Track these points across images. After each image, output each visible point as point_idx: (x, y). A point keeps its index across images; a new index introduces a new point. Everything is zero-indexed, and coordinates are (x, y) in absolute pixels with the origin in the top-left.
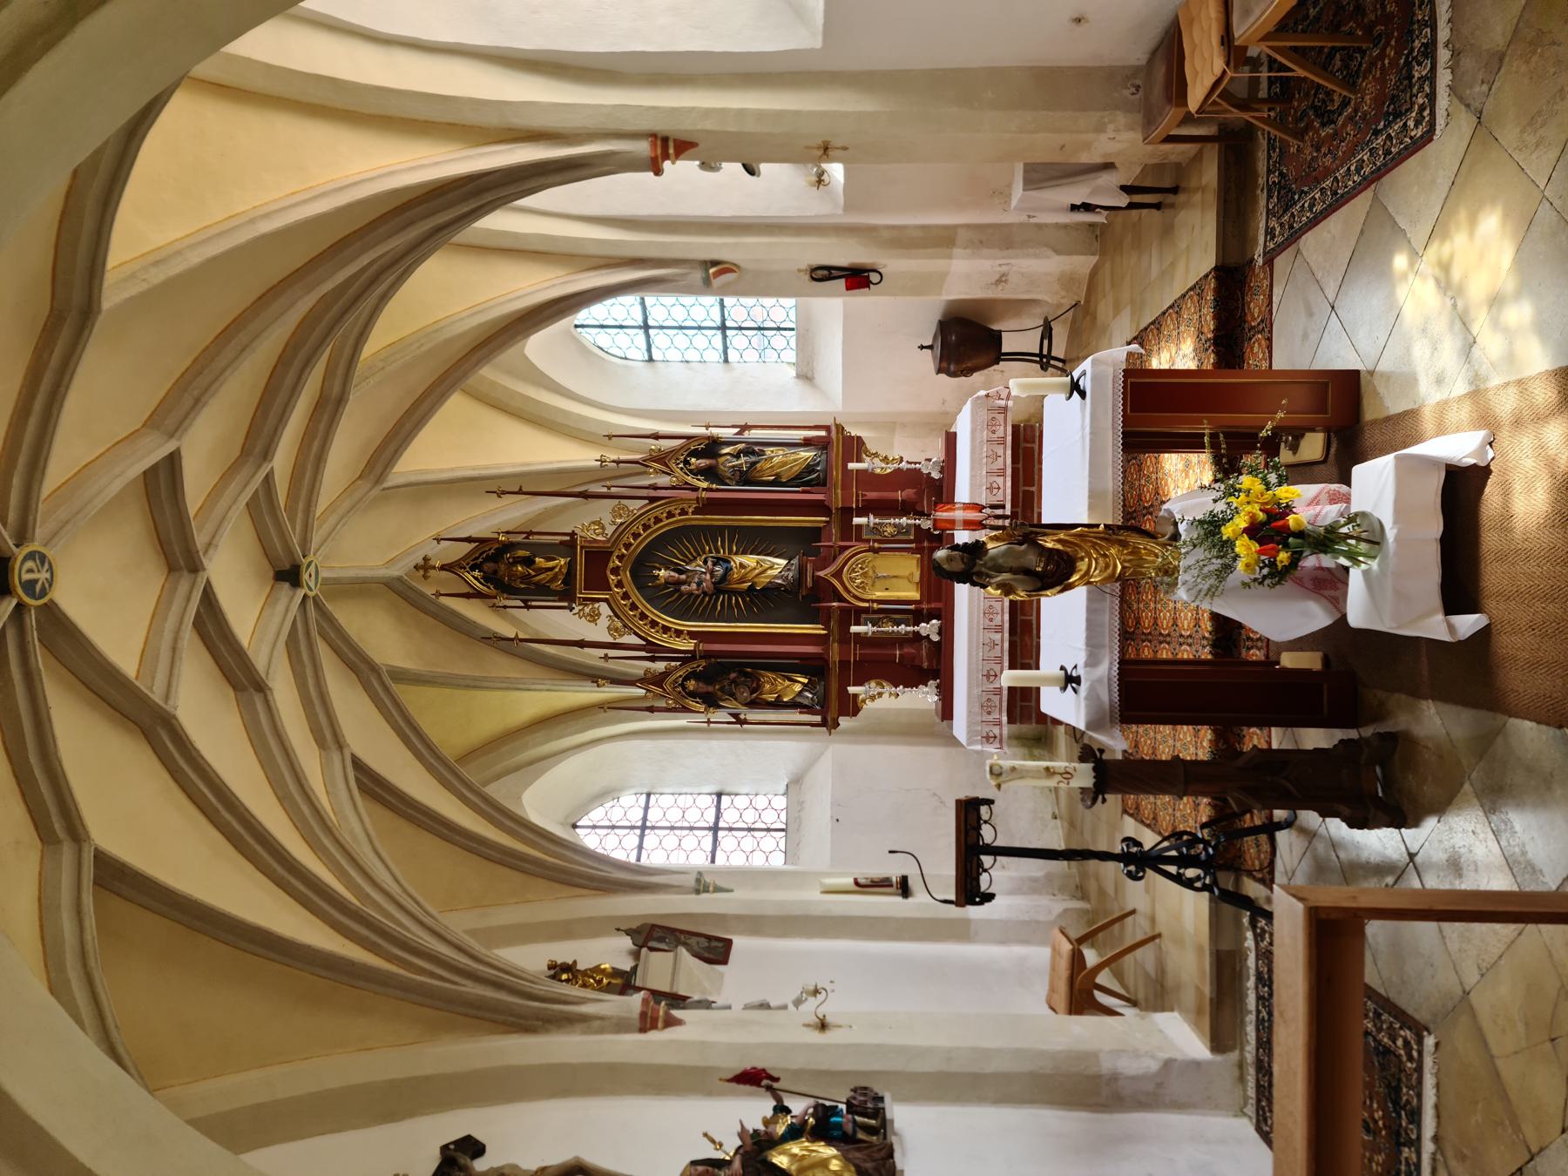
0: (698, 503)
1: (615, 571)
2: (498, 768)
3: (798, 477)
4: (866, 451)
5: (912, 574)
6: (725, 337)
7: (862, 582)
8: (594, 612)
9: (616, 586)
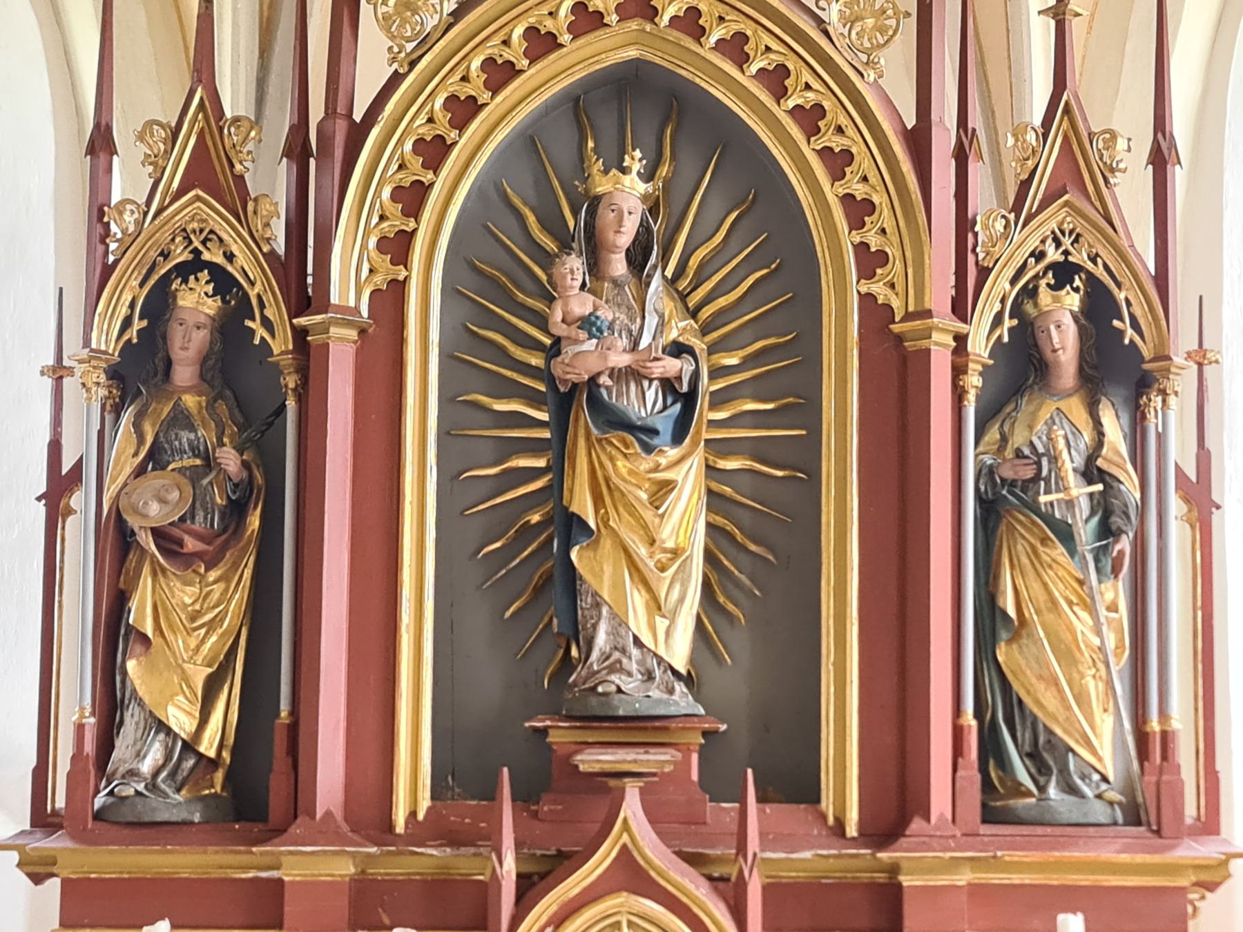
3: (1014, 706)
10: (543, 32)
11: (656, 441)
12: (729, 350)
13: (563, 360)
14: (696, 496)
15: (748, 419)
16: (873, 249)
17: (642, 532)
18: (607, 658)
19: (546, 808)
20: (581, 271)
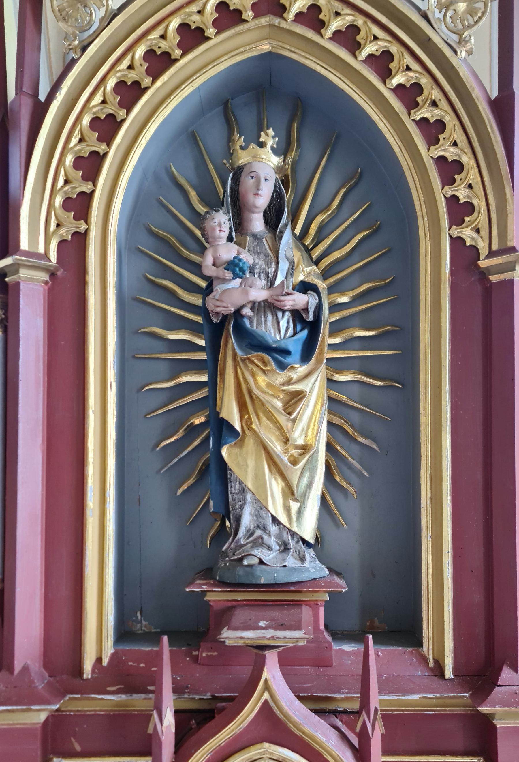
10: (193, 28)
11: (288, 360)
12: (342, 293)
13: (214, 296)
14: (320, 403)
15: (357, 344)
16: (462, 202)
17: (278, 433)
18: (252, 534)
19: (204, 655)
20: (228, 226)
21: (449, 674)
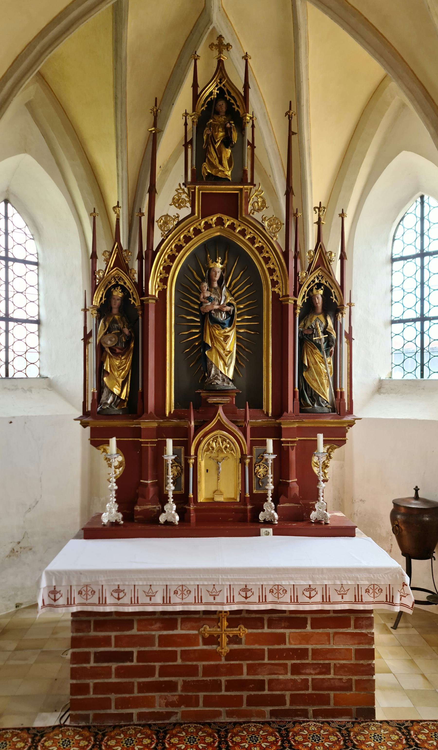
0: (283, 296)
1: (220, 222)
2: (52, 134)
3: (307, 386)
4: (333, 449)
5: (221, 494)
6: (414, 320)
7: (213, 449)
8: (182, 202)
9: (206, 223)
11: (225, 326)
12: (241, 304)
18: (214, 376)
21: (270, 415)
